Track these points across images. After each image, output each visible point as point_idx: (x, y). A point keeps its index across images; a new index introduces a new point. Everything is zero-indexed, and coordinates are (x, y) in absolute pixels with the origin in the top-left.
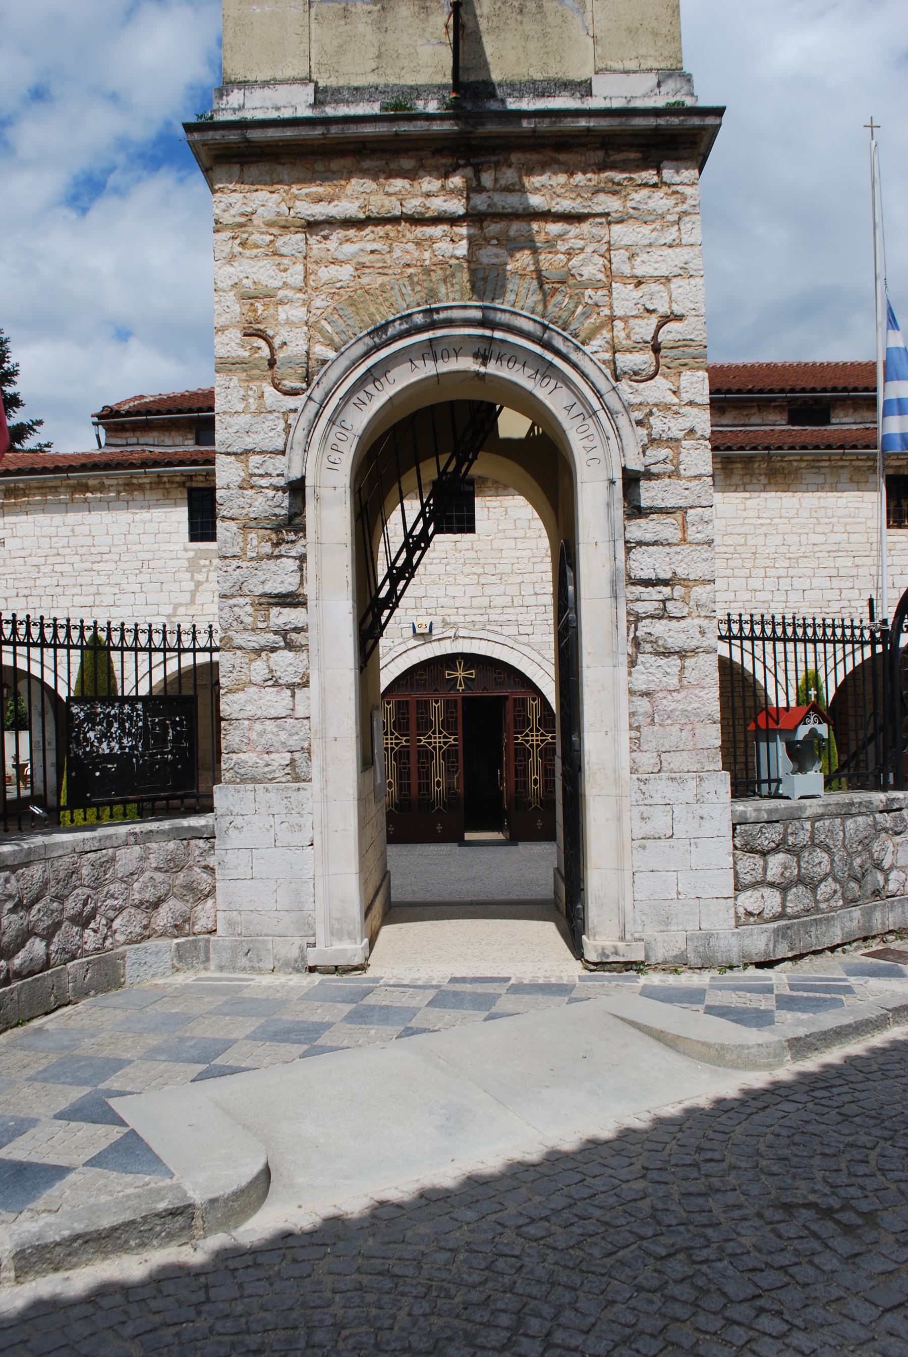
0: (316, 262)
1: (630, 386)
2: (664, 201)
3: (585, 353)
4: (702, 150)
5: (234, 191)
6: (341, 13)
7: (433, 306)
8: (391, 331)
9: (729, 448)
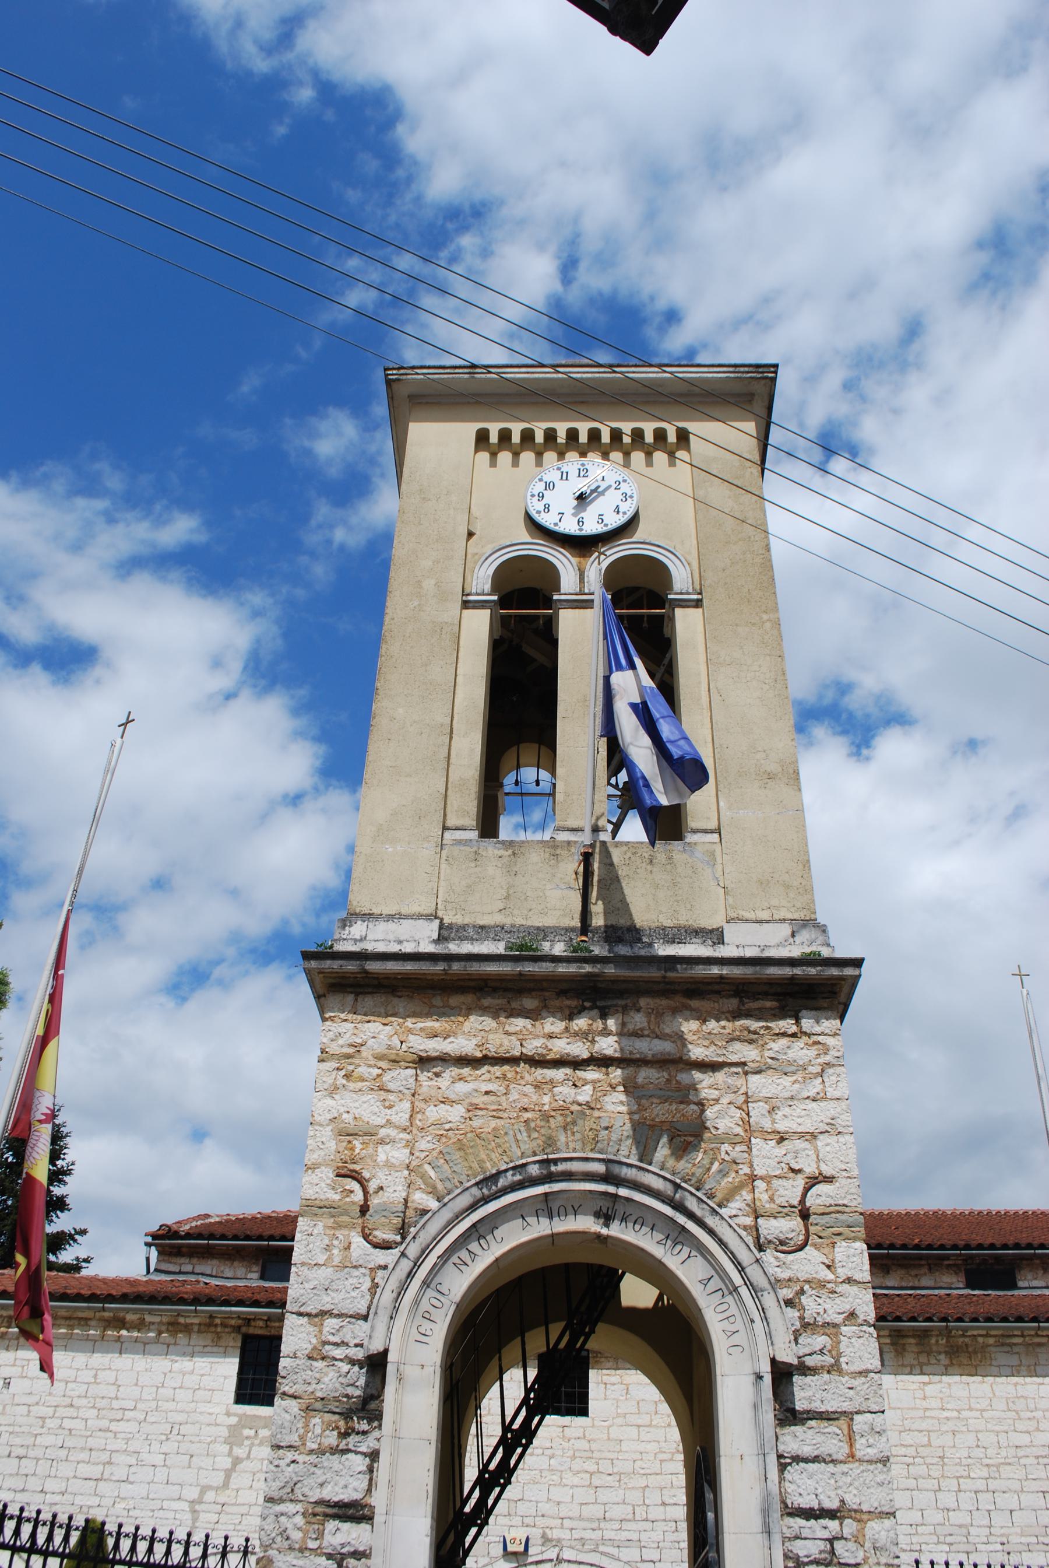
0: (425, 1100)
1: (777, 1258)
2: (805, 1051)
3: (723, 1218)
4: (843, 998)
5: (346, 1020)
6: (472, 856)
7: (551, 1156)
8: (502, 1182)
9: (898, 1319)
